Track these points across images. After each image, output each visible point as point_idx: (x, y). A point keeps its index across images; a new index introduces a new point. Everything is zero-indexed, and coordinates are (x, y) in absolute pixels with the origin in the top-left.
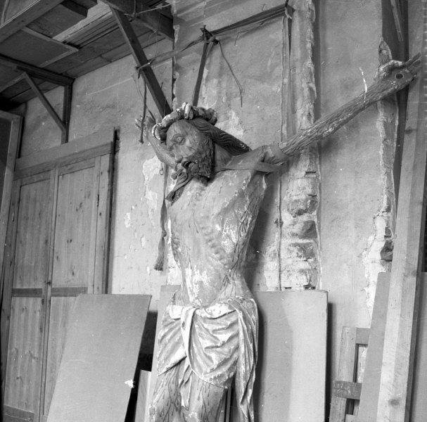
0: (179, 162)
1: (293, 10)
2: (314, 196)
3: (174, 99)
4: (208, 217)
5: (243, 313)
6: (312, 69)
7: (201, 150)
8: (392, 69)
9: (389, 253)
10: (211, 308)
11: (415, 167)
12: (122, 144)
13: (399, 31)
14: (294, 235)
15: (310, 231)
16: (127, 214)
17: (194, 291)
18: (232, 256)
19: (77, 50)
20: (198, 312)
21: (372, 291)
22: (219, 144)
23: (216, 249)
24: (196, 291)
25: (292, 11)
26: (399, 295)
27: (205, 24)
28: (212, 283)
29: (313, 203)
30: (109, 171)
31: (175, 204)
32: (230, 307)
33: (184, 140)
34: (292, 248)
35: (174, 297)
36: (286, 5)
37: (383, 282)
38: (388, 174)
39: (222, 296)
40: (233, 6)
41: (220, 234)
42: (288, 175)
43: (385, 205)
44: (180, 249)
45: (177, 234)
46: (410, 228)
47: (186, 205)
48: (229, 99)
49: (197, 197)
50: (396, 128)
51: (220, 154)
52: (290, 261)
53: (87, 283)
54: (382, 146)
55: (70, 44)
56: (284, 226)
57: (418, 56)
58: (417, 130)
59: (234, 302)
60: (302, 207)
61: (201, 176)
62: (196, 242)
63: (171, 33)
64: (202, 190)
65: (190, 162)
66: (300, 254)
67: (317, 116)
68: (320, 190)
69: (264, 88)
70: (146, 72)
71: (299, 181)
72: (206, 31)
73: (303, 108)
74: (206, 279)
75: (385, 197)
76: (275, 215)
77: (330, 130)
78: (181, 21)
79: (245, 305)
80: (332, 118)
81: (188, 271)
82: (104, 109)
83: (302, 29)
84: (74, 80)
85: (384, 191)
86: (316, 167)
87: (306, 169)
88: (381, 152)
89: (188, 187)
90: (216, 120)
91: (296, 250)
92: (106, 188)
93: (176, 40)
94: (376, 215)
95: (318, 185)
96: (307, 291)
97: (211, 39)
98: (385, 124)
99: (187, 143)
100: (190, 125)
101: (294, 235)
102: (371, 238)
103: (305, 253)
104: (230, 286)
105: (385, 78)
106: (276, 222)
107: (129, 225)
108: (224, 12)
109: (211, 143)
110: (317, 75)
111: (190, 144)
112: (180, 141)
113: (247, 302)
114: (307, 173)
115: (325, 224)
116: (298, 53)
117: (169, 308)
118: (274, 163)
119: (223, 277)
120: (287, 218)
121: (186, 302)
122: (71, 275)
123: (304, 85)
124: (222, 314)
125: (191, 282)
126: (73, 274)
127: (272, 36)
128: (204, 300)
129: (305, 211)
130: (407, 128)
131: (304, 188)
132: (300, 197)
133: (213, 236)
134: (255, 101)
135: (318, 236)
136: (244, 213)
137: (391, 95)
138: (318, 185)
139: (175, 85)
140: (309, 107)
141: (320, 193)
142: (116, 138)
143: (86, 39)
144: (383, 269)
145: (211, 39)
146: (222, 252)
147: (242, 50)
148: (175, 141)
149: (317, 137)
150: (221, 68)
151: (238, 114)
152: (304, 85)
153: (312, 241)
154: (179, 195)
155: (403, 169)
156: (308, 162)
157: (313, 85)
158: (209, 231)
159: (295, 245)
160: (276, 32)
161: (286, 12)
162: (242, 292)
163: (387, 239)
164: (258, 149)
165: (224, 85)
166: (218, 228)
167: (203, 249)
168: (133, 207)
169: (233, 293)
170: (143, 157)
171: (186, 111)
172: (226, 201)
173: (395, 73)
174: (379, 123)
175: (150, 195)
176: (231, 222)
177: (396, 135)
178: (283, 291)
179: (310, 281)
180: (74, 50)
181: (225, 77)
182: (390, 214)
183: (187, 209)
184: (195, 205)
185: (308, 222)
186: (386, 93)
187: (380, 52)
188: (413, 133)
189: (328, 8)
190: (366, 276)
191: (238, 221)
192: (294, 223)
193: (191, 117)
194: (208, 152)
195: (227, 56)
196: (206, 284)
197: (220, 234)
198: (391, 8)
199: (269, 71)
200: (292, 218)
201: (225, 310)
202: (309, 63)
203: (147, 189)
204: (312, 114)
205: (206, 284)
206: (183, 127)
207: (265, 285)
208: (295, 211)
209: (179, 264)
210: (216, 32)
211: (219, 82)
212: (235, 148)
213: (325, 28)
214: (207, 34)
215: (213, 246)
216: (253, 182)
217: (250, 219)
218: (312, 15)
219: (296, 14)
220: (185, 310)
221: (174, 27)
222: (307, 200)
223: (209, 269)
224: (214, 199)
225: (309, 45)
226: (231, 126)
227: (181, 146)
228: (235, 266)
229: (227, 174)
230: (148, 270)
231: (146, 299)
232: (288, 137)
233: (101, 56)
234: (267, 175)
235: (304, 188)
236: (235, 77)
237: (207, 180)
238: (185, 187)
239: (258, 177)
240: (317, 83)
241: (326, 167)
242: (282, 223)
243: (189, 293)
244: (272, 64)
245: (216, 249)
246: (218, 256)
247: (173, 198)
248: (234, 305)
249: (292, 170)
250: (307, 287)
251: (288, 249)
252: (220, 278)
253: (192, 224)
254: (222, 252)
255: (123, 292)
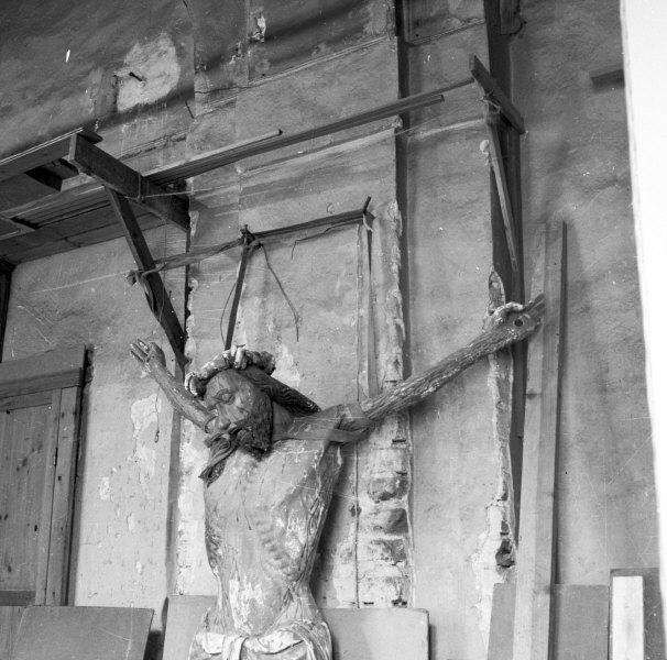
0: (225, 428)
1: (373, 218)
2: (403, 474)
3: (189, 318)
4: (266, 508)
5: (314, 645)
6: (400, 299)
7: (256, 411)
8: (509, 313)
9: (507, 557)
10: (268, 638)
11: (541, 445)
12: (97, 371)
13: (513, 259)
14: (377, 528)
15: (399, 523)
16: (104, 479)
17: (243, 614)
18: (299, 562)
19: (33, 230)
20: (247, 644)
21: (486, 610)
22: (278, 403)
23: (277, 553)
24: (245, 612)
25: (371, 219)
26: (529, 618)
27: (242, 224)
28: (268, 602)
29: (403, 484)
30: (75, 413)
31: (212, 486)
32: (295, 637)
33: (231, 399)
34: (373, 547)
35: (207, 620)
36: (365, 211)
37: (503, 600)
38: (503, 449)
39: (282, 619)
40: (283, 199)
41: (283, 532)
42: (368, 443)
43: (500, 492)
44: (220, 552)
45: (217, 530)
46: (539, 528)
47: (231, 489)
48: (278, 328)
49: (247, 478)
50: (511, 386)
51: (280, 415)
52: (371, 565)
53: (35, 587)
54: (495, 412)
55: (22, 221)
56: (362, 514)
57: (540, 298)
58: (542, 395)
59: (301, 629)
60: (388, 489)
61: (254, 448)
62: (247, 544)
63: (185, 223)
64: (255, 466)
65: (239, 430)
66: (386, 555)
67: (406, 374)
68: (411, 464)
69: (331, 318)
70: (150, 275)
71: (384, 452)
72: (248, 232)
73: (389, 353)
74: (259, 595)
75: (501, 480)
76: (350, 499)
77: (431, 390)
78: (200, 206)
79: (315, 632)
80: (432, 375)
81: (234, 584)
82: (66, 315)
83: (384, 243)
84: (14, 267)
85: (500, 472)
86: (406, 434)
87: (393, 437)
88: (494, 420)
89: (231, 461)
90: (274, 369)
91: (380, 549)
92: (71, 440)
93: (193, 232)
94: (488, 505)
95: (410, 459)
96: (395, 609)
97: (253, 242)
98: (500, 383)
99: (238, 402)
100: (240, 376)
101: (377, 528)
102: (483, 536)
103: (393, 553)
104: (294, 605)
105: (501, 325)
106: (352, 510)
107: (108, 496)
108: (269, 206)
109: (268, 401)
110: (405, 307)
111: (239, 406)
112: (224, 399)
113: (319, 628)
114: (394, 441)
115: (418, 514)
116: (379, 277)
117: (200, 637)
118: (353, 429)
119: (284, 591)
120: (366, 503)
121: (226, 627)
122: (5, 572)
123: (389, 320)
124: (283, 647)
125: (238, 600)
126: (10, 570)
127: (341, 248)
128: (256, 626)
129: (392, 496)
130: (528, 391)
131: (391, 463)
132: (384, 475)
133: (276, 533)
134: (317, 335)
135: (410, 530)
136: (314, 499)
137: (506, 348)
138: (410, 459)
139: (191, 297)
140: (396, 351)
141: (412, 469)
142: (87, 363)
143: (48, 217)
144: (500, 579)
145: (253, 242)
146: (285, 558)
147: (299, 262)
148: (219, 399)
149: (413, 398)
150: (266, 283)
151: (291, 351)
152: (389, 321)
153: (401, 537)
154: (220, 473)
155: (526, 453)
156: (396, 427)
157: (400, 322)
158: (268, 527)
159: (379, 542)
160: (348, 244)
161: (364, 219)
162: (309, 612)
163: (505, 537)
164: (331, 409)
165: (271, 306)
166: (280, 523)
167: (257, 552)
168: (114, 470)
169: (299, 615)
170: (132, 395)
171: (238, 359)
172: (291, 485)
173: (513, 319)
174: (491, 381)
175: (142, 452)
176: (298, 514)
177: (511, 395)
178: (361, 608)
179: (401, 594)
180: (27, 230)
181: (271, 296)
182: (506, 503)
183: (233, 495)
184: (245, 489)
185: (396, 511)
186: (502, 344)
187: (490, 284)
188: (535, 400)
189: (418, 219)
190: (477, 587)
191: (307, 513)
192: (377, 512)
193: (243, 366)
194: (265, 415)
195: (276, 268)
196: (261, 603)
197: (283, 532)
198: (504, 229)
199: (338, 295)
200: (374, 504)
201: (288, 640)
202: (395, 291)
203: (139, 445)
204: (400, 360)
205: (261, 603)
206: (231, 379)
207: (334, 598)
208: (378, 494)
209: (216, 572)
210: (262, 235)
211: (263, 302)
212: (297, 406)
213: (414, 244)
214: (249, 236)
215: (273, 549)
216: (326, 459)
217: (322, 509)
218: (398, 226)
219: (376, 223)
220: (228, 642)
221: (190, 214)
222: (395, 480)
223: (264, 581)
224: (274, 482)
225: (395, 268)
226: (286, 374)
227: (226, 406)
228: (299, 577)
229: (289, 444)
230: (139, 566)
231: (143, 614)
232: (372, 395)
233: (66, 238)
234: (341, 445)
235: (391, 463)
236: (287, 299)
237: (260, 452)
238: (228, 461)
239: (331, 450)
240: (406, 319)
241: (420, 434)
242: (359, 510)
243: (234, 615)
244: (341, 287)
245: (277, 553)
246: (279, 562)
247: (210, 476)
248: (301, 635)
249: (374, 438)
250: (395, 603)
251: (369, 548)
252: (280, 594)
253: (242, 518)
254: (285, 558)
255: (91, 603)
